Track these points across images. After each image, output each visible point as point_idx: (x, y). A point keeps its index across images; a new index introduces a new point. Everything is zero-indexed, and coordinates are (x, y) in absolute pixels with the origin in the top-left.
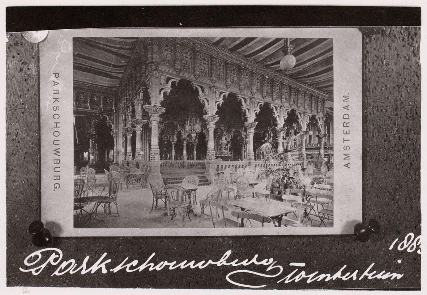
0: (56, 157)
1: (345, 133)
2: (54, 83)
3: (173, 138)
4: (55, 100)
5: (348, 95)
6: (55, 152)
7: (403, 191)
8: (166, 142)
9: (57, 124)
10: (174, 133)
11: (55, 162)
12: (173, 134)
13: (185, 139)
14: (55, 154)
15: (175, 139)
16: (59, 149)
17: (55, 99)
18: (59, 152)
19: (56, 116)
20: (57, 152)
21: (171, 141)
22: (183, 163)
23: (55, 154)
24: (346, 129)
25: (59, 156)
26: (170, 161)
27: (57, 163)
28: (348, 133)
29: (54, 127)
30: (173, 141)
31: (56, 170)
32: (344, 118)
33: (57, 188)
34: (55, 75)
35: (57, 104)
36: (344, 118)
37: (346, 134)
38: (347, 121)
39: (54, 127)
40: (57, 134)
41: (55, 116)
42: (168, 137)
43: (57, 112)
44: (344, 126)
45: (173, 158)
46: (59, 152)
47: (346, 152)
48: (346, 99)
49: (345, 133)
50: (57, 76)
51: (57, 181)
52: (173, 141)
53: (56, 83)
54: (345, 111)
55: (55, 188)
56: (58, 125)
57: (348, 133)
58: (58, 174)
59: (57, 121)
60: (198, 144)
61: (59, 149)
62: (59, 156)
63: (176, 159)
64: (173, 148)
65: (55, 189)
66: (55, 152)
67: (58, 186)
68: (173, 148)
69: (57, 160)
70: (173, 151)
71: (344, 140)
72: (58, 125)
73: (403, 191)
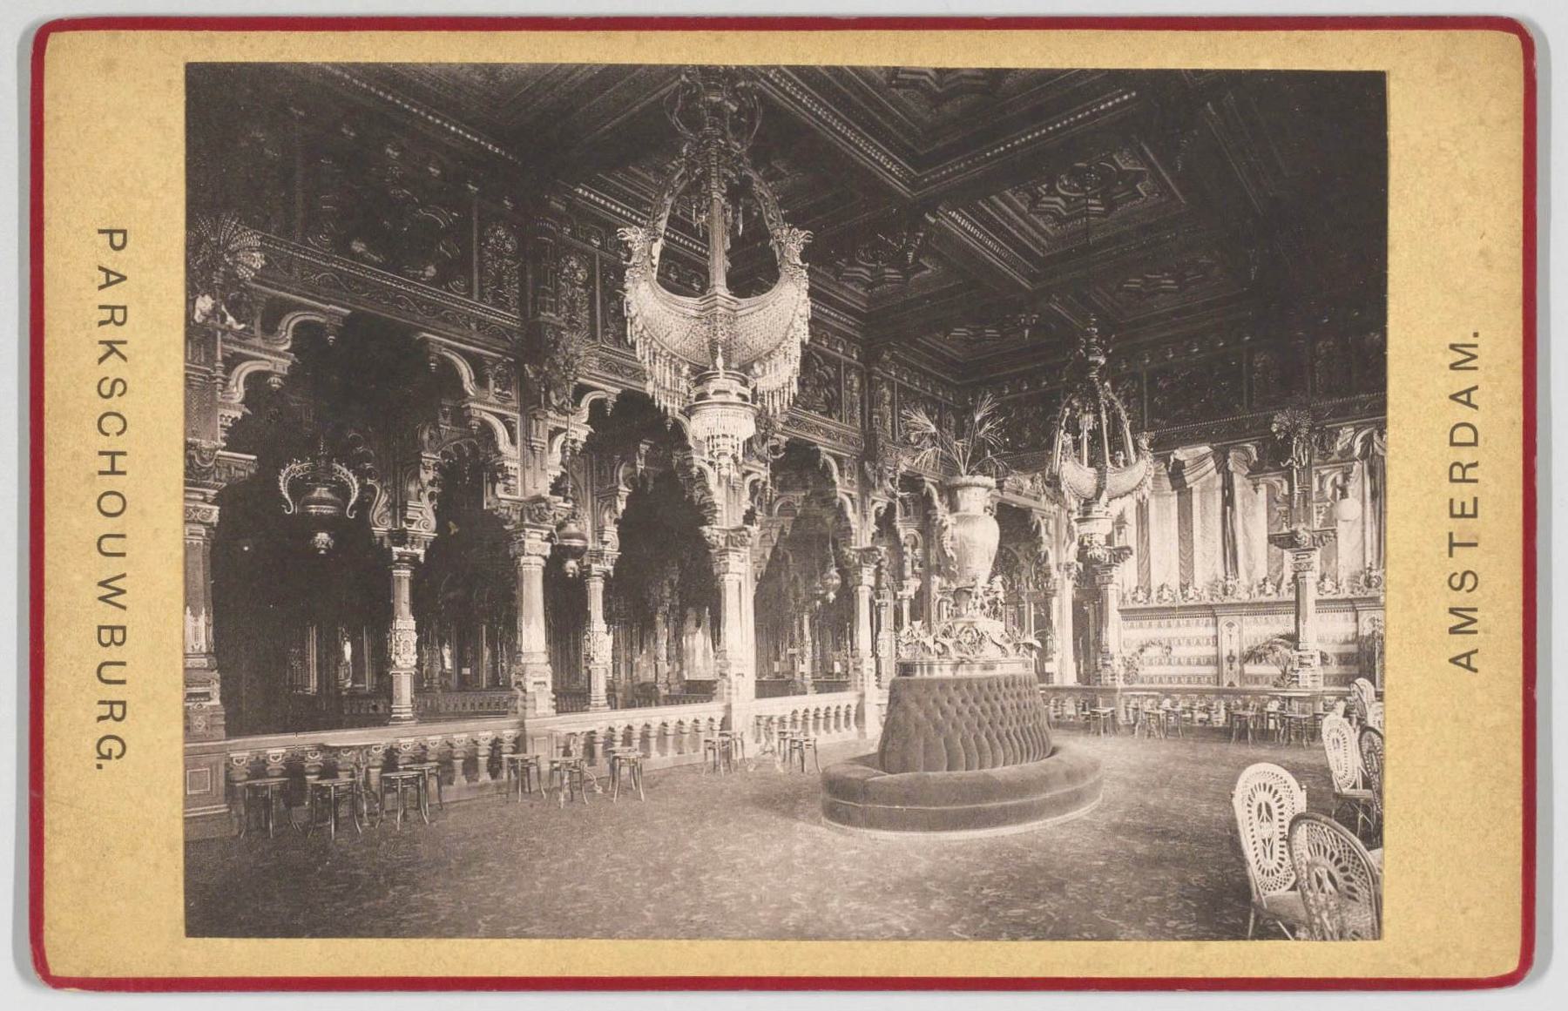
0: (112, 616)
1: (1457, 511)
2: (103, 274)
3: (398, 507)
5: (1473, 341)
6: (107, 592)
8: (322, 537)
9: (117, 458)
11: (106, 638)
13: (534, 508)
14: (103, 599)
15: (423, 520)
16: (124, 576)
17: (109, 343)
18: (121, 592)
19: (112, 424)
20: (111, 591)
21: (380, 530)
22: (519, 744)
23: (103, 599)
24: (1463, 493)
25: (124, 608)
26: (376, 738)
27: (112, 639)
28: (1469, 510)
29: (101, 473)
30: (400, 537)
31: (108, 673)
33: (109, 757)
34: (106, 237)
35: (113, 367)
36: (1452, 444)
37: (1463, 515)
38: (1466, 456)
39: (101, 473)
40: (112, 504)
41: (105, 420)
42: (342, 490)
43: (114, 404)
44: (1452, 480)
45: (405, 690)
46: (121, 592)
47: (1459, 599)
48: (1465, 357)
49: (1457, 511)
50: (118, 239)
51: (110, 727)
52: (400, 537)
53: (113, 278)
55: (103, 757)
57: (1469, 510)
58: (114, 693)
60: (618, 564)
61: (124, 576)
62: (124, 608)
63: (433, 701)
64: (404, 595)
65: (103, 762)
66: (107, 592)
68: (404, 595)
69: (112, 628)
71: (1452, 545)
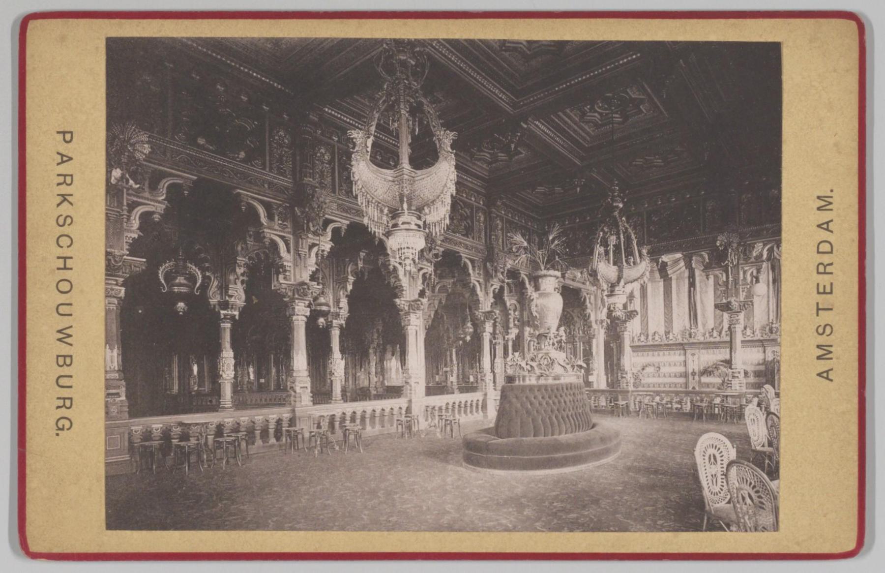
0: (65, 350)
1: (821, 290)
3: (224, 288)
4: (61, 198)
5: (830, 194)
7: (636, 339)
9: (68, 261)
10: (230, 265)
12: (224, 266)
13: (300, 289)
14: (60, 340)
15: (238, 295)
16: (71, 327)
17: (63, 195)
19: (65, 241)
20: (64, 336)
22: (292, 422)
23: (60, 340)
24: (825, 280)
25: (71, 345)
26: (211, 419)
28: (828, 290)
29: (58, 269)
30: (225, 305)
32: (818, 252)
34: (62, 135)
35: (65, 209)
36: (818, 252)
37: (824, 293)
38: (826, 259)
39: (58, 269)
40: (65, 286)
41: (61, 239)
42: (192, 279)
43: (66, 230)
44: (818, 273)
45: (227, 391)
49: (821, 290)
50: (68, 137)
51: (64, 412)
52: (225, 305)
54: (824, 235)
55: (59, 429)
56: (69, 263)
57: (828, 290)
58: (65, 393)
59: (66, 252)
60: (348, 320)
61: (71, 327)
65: (59, 432)
67: (67, 424)
69: (65, 356)
70: (228, 356)
71: (818, 309)
72: (69, 263)
73: (636, 339)
